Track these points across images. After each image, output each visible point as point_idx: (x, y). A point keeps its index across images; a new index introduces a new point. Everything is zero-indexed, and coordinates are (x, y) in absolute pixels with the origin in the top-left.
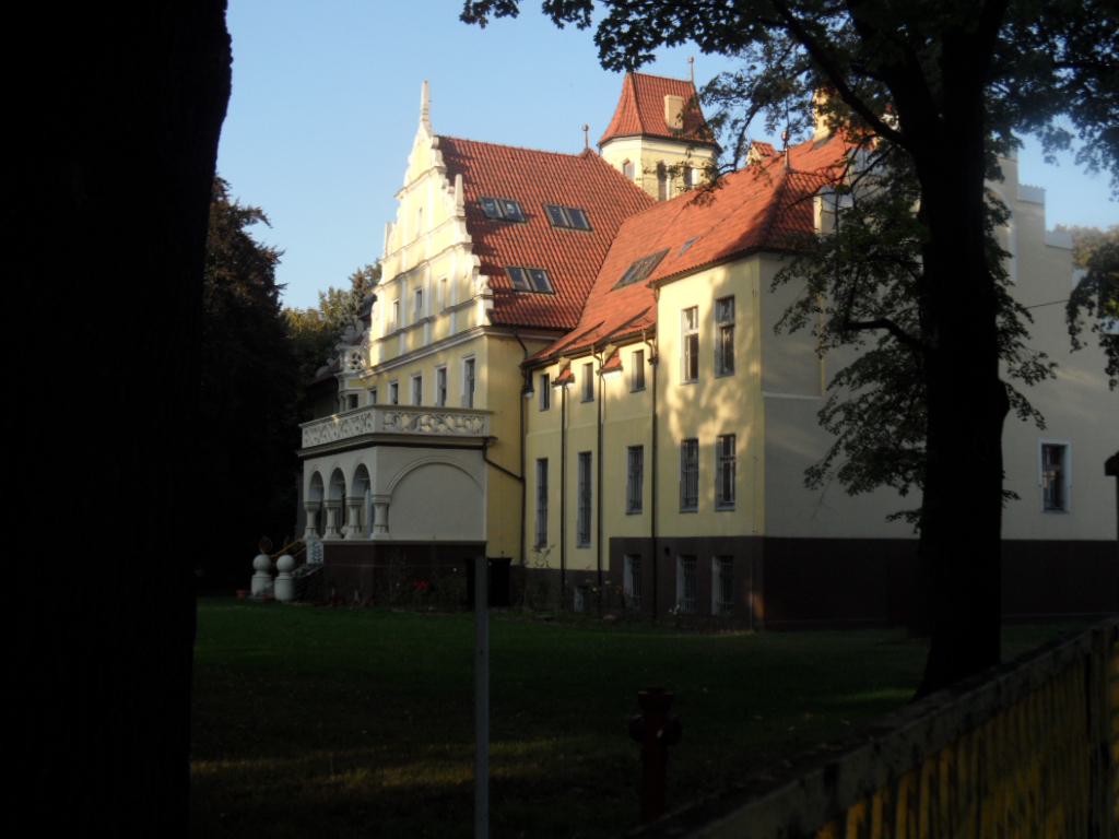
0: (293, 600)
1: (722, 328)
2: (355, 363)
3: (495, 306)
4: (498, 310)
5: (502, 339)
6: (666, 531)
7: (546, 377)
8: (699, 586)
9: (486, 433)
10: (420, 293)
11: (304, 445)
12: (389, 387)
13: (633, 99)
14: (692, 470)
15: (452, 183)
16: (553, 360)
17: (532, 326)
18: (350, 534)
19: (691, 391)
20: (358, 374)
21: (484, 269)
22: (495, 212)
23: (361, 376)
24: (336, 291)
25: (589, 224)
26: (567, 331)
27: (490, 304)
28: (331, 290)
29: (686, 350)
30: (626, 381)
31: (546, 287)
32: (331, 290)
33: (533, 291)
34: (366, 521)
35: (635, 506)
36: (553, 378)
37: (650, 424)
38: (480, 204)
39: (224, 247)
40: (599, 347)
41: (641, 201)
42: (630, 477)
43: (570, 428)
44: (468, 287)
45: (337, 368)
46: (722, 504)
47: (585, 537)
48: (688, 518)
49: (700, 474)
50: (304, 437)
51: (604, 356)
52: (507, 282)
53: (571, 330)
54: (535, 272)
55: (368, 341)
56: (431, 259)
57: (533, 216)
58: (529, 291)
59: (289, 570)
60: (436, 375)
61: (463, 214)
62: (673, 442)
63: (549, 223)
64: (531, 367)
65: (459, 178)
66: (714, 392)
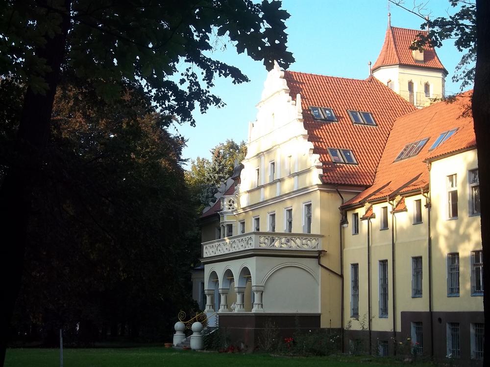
0: (203, 349)
1: (473, 187)
2: (231, 205)
3: (324, 173)
4: (326, 174)
5: (328, 192)
6: (437, 308)
7: (356, 215)
8: (461, 342)
9: (320, 249)
10: (273, 164)
11: (205, 256)
12: (253, 219)
13: (392, 43)
14: (454, 271)
15: (294, 98)
16: (361, 205)
17: (346, 186)
18: (237, 309)
19: (453, 224)
20: (232, 212)
21: (316, 151)
22: (319, 115)
23: (235, 214)
24: (201, 159)
25: (375, 121)
26: (367, 187)
27: (321, 171)
28: (198, 159)
29: (449, 200)
30: (410, 218)
31: (352, 161)
32: (198, 159)
33: (345, 163)
34: (216, 302)
35: (417, 293)
36: (360, 216)
37: (426, 244)
38: (310, 111)
39: (156, 138)
40: (392, 198)
41: (407, 108)
42: (414, 275)
43: (373, 246)
44: (306, 162)
45: (218, 208)
46: (475, 292)
47: (384, 311)
48: (453, 300)
49: (460, 273)
50: (205, 251)
51: (395, 203)
52: (330, 158)
53: (370, 186)
54: (345, 152)
55: (238, 192)
56: (281, 144)
57: (342, 118)
58: (342, 163)
59: (199, 331)
60: (285, 214)
61: (301, 117)
62: (442, 255)
63: (352, 122)
64: (346, 209)
65: (298, 96)
66: (469, 225)
